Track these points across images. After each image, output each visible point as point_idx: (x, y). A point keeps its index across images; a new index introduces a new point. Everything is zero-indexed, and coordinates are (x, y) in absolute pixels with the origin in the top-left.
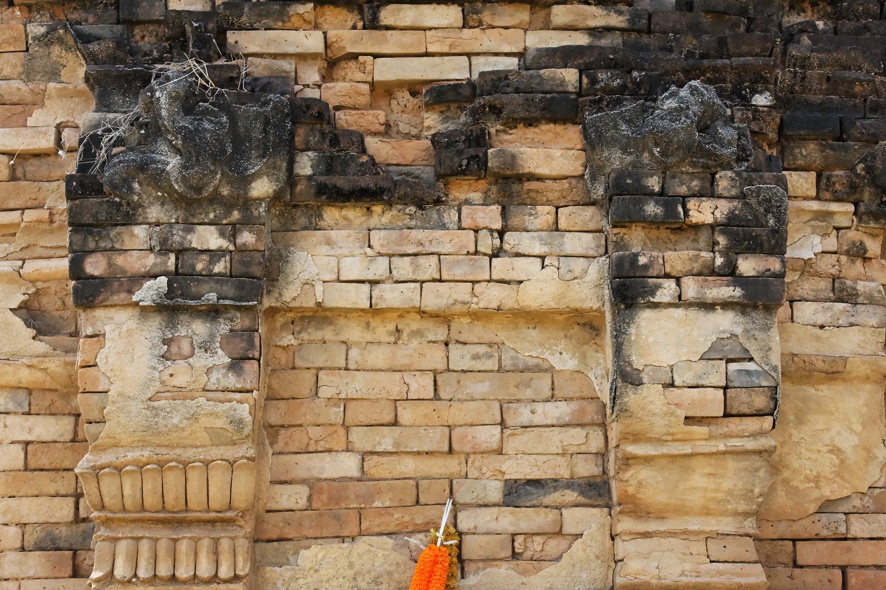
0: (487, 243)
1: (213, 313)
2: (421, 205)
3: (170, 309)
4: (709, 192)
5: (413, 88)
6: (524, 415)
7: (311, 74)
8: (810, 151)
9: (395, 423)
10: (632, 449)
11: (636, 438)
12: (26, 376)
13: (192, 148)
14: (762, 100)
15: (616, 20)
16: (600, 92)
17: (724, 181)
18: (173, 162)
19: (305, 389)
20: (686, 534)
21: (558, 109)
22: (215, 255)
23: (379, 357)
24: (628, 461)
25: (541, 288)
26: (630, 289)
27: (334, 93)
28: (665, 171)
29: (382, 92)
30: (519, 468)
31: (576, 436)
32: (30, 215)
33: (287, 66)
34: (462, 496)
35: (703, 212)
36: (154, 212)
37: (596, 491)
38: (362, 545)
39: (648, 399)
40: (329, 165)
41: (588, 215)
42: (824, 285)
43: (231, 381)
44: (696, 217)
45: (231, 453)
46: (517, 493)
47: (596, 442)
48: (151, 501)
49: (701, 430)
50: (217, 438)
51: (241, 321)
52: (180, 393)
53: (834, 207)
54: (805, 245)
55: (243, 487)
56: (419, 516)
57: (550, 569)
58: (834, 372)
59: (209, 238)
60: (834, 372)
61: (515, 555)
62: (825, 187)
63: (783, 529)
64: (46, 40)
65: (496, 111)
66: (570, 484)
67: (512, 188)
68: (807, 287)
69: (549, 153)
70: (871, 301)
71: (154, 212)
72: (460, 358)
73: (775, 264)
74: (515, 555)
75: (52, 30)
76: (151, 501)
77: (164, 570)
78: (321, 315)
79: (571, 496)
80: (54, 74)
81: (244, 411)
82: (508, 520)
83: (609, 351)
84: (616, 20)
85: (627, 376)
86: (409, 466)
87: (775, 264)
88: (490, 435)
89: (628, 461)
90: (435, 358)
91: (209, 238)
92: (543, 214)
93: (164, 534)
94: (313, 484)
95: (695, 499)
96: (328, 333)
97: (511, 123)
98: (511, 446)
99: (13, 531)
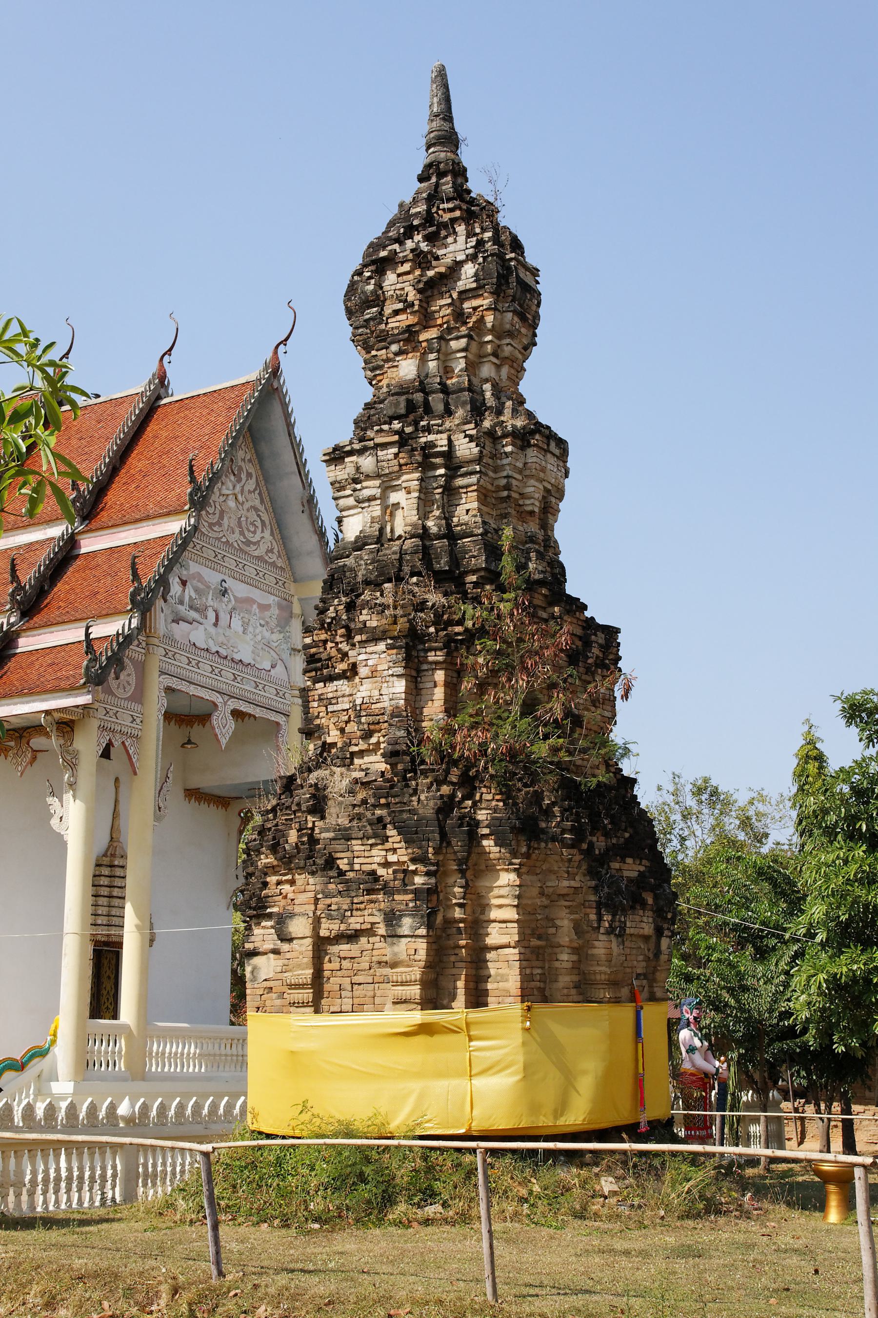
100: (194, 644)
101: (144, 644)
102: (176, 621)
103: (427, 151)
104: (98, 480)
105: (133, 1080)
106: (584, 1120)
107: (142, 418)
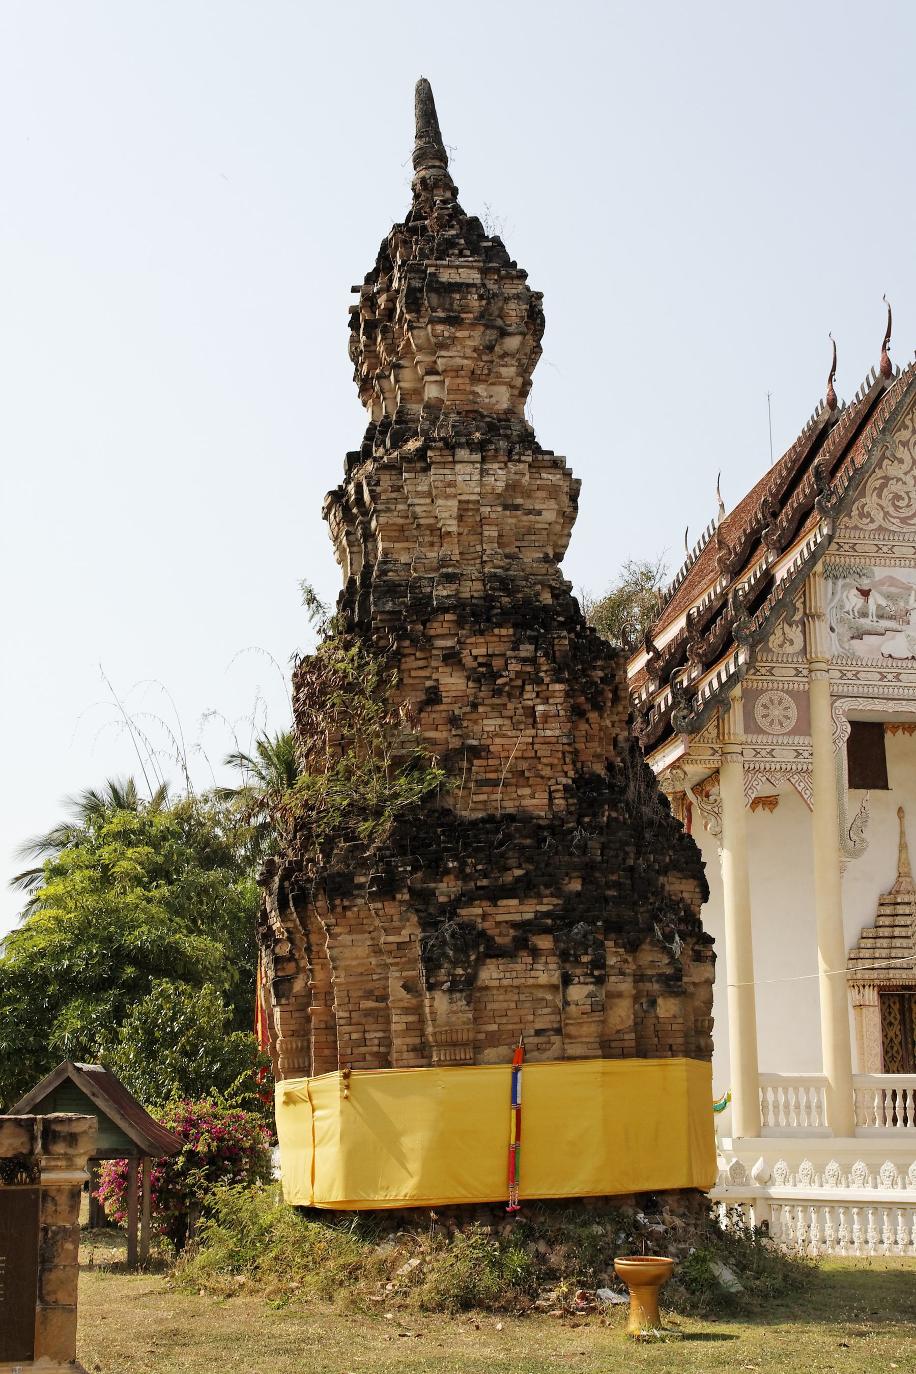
0: (529, 967)
1: (461, 991)
2: (511, 957)
3: (451, 991)
4: (586, 954)
5: (506, 922)
6: (539, 1012)
7: (479, 920)
8: (613, 936)
9: (506, 1015)
10: (568, 1021)
11: (569, 1019)
12: (406, 1005)
13: (456, 950)
14: (599, 924)
15: (560, 902)
16: (558, 923)
17: (590, 950)
18: (451, 953)
19: (483, 1008)
20: (582, 1042)
21: (547, 931)
22: (461, 975)
23: (501, 998)
24: (567, 1025)
25: (543, 979)
26: (567, 980)
27: (487, 925)
28: (575, 949)
29: (498, 924)
30: (539, 1026)
31: (553, 1017)
32: (403, 959)
33: (473, 918)
34: (525, 1034)
35: (585, 959)
36: (446, 965)
37: (558, 1031)
38: (501, 1048)
39: (572, 1009)
40: (487, 948)
41: (555, 959)
42: (617, 971)
43: (467, 1008)
44: (583, 960)
45: (468, 1027)
46: (538, 1033)
47: (558, 1019)
48: (449, 1040)
49: (585, 1016)
50: (464, 1023)
51: (468, 992)
52: (455, 1012)
53: (619, 950)
54: (612, 961)
55: (471, 1035)
56: (514, 1040)
57: (548, 1053)
58: (620, 995)
59: (460, 971)
60: (620, 995)
61: (538, 1049)
62: (617, 945)
63: (606, 1038)
64: (406, 911)
65: (530, 931)
66: (552, 1029)
67: (535, 953)
68: (612, 972)
69: (544, 942)
70: (629, 975)
71: (446, 965)
72: (522, 997)
73: (603, 972)
74: (538, 1049)
75: (408, 909)
76: (449, 1040)
77: (453, 1058)
78: (487, 988)
79: (552, 1033)
80: (408, 920)
81: (471, 1016)
82: (536, 1040)
83: (561, 995)
84: (560, 902)
85: (566, 1003)
86: (510, 1027)
87: (603, 972)
88: (531, 1018)
89: (567, 1025)
90: (516, 998)
91: (460, 971)
92: (543, 959)
93: (452, 1048)
94: (487, 1033)
95: (584, 1033)
96: (488, 993)
97: (534, 935)
98: (536, 1020)
99: (405, 1047)
100: (890, 656)
101: (805, 672)
102: (859, 636)
103: (415, 169)
104: (800, 504)
105: (835, 1137)
106: (406, 1196)
107: (859, 421)
